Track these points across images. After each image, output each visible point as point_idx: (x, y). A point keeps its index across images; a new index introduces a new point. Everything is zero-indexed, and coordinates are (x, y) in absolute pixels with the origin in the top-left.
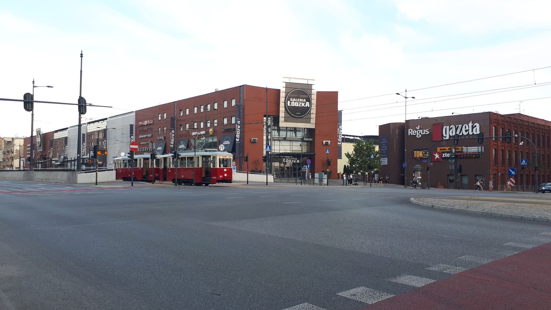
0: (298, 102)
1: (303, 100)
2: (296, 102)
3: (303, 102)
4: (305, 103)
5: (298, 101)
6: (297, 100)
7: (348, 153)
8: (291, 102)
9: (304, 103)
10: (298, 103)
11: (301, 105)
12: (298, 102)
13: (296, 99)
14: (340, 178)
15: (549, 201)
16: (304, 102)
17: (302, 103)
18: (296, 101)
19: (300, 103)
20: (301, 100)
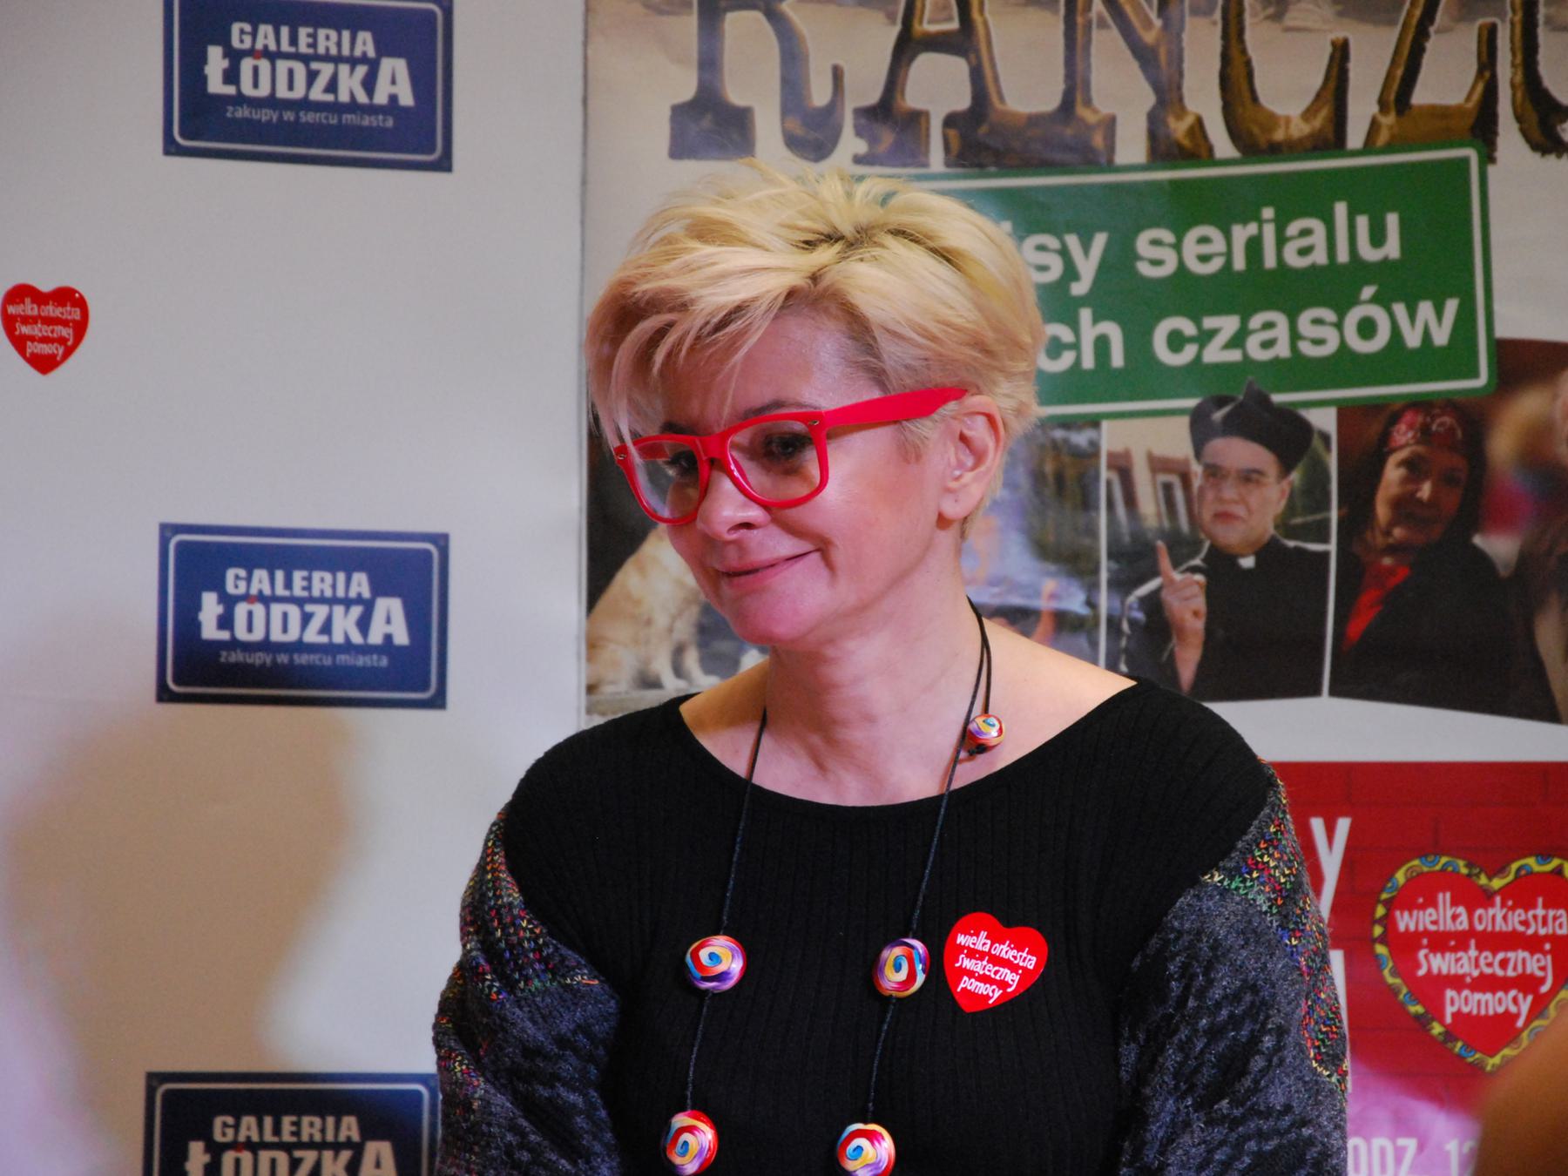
0: (299, 602)
1: (330, 1120)
2: (288, 56)
3: (347, 603)
4: (369, 607)
5: (287, 1137)
6: (277, 1130)
7: (693, 1134)
8: (229, 602)
9: (356, 611)
10: (294, 612)
11: (326, 628)
12: (299, 602)
13: (285, 31)
14: (768, 127)
15: (1233, 5)
16: (359, 600)
17: (328, 1155)
18: (269, 1137)
19: (320, 612)
20: (327, 40)
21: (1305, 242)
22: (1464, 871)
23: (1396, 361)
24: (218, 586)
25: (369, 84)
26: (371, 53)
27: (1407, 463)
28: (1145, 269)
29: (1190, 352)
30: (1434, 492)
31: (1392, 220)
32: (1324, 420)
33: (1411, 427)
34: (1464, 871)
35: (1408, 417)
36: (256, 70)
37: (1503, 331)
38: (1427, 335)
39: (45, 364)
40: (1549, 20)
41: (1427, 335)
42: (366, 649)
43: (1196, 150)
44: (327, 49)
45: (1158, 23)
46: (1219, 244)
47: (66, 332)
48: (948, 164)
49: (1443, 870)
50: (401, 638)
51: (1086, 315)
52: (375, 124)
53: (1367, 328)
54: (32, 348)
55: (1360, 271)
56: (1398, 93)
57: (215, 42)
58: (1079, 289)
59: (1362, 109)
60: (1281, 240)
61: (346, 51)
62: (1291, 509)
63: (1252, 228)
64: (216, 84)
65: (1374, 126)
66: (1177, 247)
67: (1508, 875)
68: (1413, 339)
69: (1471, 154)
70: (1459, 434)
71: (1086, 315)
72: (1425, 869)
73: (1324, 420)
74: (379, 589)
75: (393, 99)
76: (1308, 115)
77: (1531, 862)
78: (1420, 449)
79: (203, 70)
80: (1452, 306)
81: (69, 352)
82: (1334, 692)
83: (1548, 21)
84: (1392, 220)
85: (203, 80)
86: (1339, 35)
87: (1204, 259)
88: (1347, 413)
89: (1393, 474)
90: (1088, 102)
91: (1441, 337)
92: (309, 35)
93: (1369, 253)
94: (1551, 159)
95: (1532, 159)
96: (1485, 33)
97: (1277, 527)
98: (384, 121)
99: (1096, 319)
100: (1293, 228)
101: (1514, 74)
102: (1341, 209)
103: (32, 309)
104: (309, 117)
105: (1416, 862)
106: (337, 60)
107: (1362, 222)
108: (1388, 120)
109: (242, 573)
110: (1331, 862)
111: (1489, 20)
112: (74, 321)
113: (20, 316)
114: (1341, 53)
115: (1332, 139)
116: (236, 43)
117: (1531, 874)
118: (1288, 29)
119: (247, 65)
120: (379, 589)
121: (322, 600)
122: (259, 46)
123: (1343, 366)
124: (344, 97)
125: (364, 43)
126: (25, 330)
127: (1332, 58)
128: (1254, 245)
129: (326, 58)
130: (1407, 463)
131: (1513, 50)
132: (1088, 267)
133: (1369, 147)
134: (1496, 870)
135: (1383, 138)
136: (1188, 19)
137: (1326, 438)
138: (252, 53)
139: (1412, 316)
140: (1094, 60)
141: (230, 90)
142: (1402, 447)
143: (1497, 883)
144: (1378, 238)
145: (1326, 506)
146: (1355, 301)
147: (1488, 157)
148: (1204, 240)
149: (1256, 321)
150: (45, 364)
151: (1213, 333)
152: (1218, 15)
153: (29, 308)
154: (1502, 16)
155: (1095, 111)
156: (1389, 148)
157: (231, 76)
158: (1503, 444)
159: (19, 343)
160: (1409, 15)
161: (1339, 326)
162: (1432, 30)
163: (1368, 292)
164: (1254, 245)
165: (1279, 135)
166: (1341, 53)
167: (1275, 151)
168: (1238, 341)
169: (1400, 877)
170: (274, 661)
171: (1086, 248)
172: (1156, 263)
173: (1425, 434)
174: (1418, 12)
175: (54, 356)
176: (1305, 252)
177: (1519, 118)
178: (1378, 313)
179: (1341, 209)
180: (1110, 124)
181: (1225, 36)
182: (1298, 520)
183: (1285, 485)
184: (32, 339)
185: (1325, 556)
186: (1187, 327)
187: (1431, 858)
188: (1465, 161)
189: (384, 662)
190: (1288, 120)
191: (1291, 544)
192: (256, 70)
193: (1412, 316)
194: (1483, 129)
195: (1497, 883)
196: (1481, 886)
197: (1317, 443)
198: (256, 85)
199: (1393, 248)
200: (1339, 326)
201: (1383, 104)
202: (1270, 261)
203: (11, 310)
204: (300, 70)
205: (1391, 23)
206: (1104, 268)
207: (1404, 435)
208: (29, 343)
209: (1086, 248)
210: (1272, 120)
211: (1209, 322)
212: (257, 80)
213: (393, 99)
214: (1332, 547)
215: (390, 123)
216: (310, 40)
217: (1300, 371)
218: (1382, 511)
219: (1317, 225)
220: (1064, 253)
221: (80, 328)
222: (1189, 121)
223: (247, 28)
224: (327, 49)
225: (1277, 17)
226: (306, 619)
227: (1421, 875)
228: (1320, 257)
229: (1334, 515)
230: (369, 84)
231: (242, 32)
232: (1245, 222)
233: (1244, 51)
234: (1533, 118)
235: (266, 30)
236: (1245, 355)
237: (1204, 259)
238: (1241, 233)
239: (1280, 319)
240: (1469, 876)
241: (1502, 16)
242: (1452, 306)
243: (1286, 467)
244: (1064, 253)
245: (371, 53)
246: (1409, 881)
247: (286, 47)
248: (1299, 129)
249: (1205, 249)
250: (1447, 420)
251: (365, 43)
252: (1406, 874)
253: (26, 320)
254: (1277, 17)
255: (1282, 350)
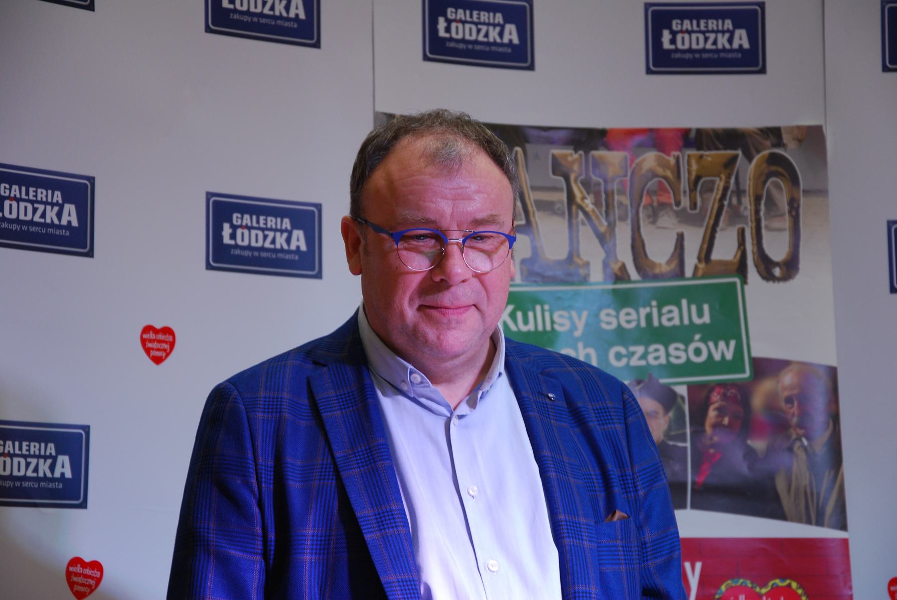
10: (701, 37)
16: (728, 31)
21: (670, 316)
22: (750, 585)
23: (710, 366)
24: (669, 27)
25: (501, 34)
26: (54, 453)
27: (718, 409)
28: (604, 326)
29: (624, 361)
30: (730, 422)
31: (706, 307)
32: (682, 390)
33: (719, 393)
34: (750, 585)
35: (717, 390)
36: (243, 234)
37: (755, 354)
38: (723, 355)
39: (158, 360)
40: (766, 227)
41: (723, 355)
42: (732, 51)
43: (621, 276)
44: (271, 226)
45: (605, 223)
46: (634, 316)
47: (166, 346)
48: (522, 280)
49: (741, 585)
50: (746, 45)
51: (580, 345)
52: (291, 258)
53: (698, 352)
54: (153, 353)
55: (693, 328)
56: (706, 254)
57: (227, 222)
58: (578, 334)
59: (691, 261)
60: (660, 315)
61: (279, 227)
62: (670, 429)
63: (648, 310)
64: (442, 33)
65: (696, 268)
66: (617, 317)
67: (768, 588)
68: (717, 357)
69: (737, 280)
70: (739, 397)
71: (580, 345)
72: (734, 585)
73: (682, 390)
74: (736, 26)
75: (511, 41)
76: (669, 262)
77: (778, 582)
78: (723, 403)
79: (221, 233)
80: (733, 343)
81: (168, 355)
82: (694, 506)
83: (766, 227)
84: (706, 307)
85: (221, 237)
86: (680, 230)
87: (628, 322)
88: (691, 387)
89: (712, 414)
90: (578, 256)
91: (729, 356)
92: (27, 446)
93: (697, 321)
94: (771, 284)
95: (763, 283)
96: (740, 231)
97: (665, 436)
98: (58, 485)
99: (585, 346)
100: (665, 310)
101: (753, 248)
102: (684, 302)
103: (153, 336)
104: (478, 47)
105: (729, 582)
106: (488, 24)
107: (694, 308)
108: (702, 266)
109: (679, 21)
110: (694, 581)
111: (741, 226)
112: (170, 342)
113: (148, 339)
114: (681, 238)
115: (680, 273)
116: (235, 222)
117: (778, 587)
118: (658, 228)
119: (454, 25)
120: (736, 26)
121: (713, 31)
122: (244, 224)
123: (688, 368)
124: (278, 246)
125: (286, 224)
126: (150, 345)
127: (677, 240)
128: (649, 317)
129: (271, 229)
130: (717, 409)
131: (752, 238)
132: (581, 325)
133: (695, 276)
134: (763, 585)
135: (700, 273)
136: (618, 223)
137: (683, 398)
138: (241, 226)
139: (716, 346)
140: (581, 239)
141: (232, 242)
142: (715, 402)
143: (764, 591)
144: (700, 314)
145: (684, 426)
146: (692, 340)
147: (744, 281)
148: (628, 314)
149: (652, 348)
150: (158, 360)
151: (633, 353)
152: (629, 221)
153: (151, 335)
154: (747, 224)
155: (581, 259)
156: (704, 277)
157: (448, 30)
158: (758, 401)
159: (148, 351)
160: (708, 223)
161: (686, 351)
162: (718, 229)
163: (697, 337)
164: (649, 317)
165: (657, 271)
166: (681, 238)
167: (656, 277)
168: (644, 356)
169: (723, 588)
170: (694, 57)
171: (580, 317)
172: (609, 323)
173: (724, 397)
174: (712, 222)
175: (161, 357)
176: (670, 320)
177: (756, 266)
178: (702, 346)
179: (684, 302)
180: (587, 264)
181: (633, 230)
182: (673, 433)
183: (667, 418)
184: (153, 349)
185: (685, 448)
186: (623, 350)
187: (736, 580)
188: (734, 284)
189: (740, 55)
190: (660, 265)
191: (671, 443)
192: (243, 234)
193: (716, 346)
194: (741, 269)
195: (764, 591)
196: (758, 592)
197: (679, 400)
198: (243, 240)
199: (706, 319)
200: (686, 351)
201: (699, 259)
202: (656, 323)
203: (145, 336)
204: (474, 28)
205: (701, 226)
206: (587, 324)
207: (715, 397)
208: (151, 351)
209: (580, 317)
210: (653, 265)
211: (632, 349)
212: (459, 32)
213: (511, 41)
214: (688, 444)
215: (61, 486)
216: (27, 448)
217: (673, 370)
218: (708, 429)
219: (675, 309)
220: (571, 318)
221: (172, 345)
222: (619, 264)
223: (239, 216)
224: (271, 226)
225: (654, 222)
226: (706, 39)
227: (732, 588)
228: (677, 322)
229: (688, 431)
230: (501, 34)
231: (237, 217)
232: (644, 306)
233: (640, 236)
234: (762, 267)
235: (460, 11)
236: (648, 363)
237: (628, 322)
238: (643, 312)
239: (661, 348)
240: (752, 588)
241: (747, 224)
242: (733, 343)
243: (667, 410)
244: (571, 318)
245: (289, 228)
246: (727, 590)
247: (255, 224)
248: (665, 269)
249: (629, 318)
250: (734, 391)
251: (499, 18)
252: (726, 586)
253: (151, 341)
254: (654, 222)
255: (663, 360)
